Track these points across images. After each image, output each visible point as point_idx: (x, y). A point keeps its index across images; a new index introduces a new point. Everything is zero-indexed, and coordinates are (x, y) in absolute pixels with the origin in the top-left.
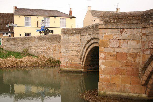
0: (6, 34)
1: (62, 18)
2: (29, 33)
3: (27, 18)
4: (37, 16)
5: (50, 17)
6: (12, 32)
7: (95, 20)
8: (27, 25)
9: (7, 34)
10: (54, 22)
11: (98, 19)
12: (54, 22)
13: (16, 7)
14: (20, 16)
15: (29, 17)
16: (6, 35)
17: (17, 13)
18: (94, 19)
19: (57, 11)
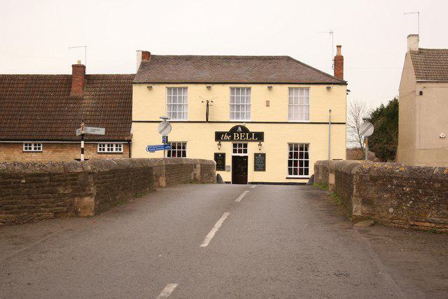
0: (106, 148)
1: (297, 89)
2: (179, 143)
3: (243, 93)
4: (209, 83)
5: (312, 86)
6: (125, 141)
7: (424, 91)
8: (174, 115)
9: (110, 148)
10: (268, 102)
11: (435, 85)
12: (268, 102)
13: (146, 55)
14: (150, 85)
15: (180, 89)
16: (106, 151)
17: (146, 77)
18: (420, 87)
19: (289, 59)
